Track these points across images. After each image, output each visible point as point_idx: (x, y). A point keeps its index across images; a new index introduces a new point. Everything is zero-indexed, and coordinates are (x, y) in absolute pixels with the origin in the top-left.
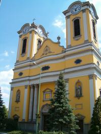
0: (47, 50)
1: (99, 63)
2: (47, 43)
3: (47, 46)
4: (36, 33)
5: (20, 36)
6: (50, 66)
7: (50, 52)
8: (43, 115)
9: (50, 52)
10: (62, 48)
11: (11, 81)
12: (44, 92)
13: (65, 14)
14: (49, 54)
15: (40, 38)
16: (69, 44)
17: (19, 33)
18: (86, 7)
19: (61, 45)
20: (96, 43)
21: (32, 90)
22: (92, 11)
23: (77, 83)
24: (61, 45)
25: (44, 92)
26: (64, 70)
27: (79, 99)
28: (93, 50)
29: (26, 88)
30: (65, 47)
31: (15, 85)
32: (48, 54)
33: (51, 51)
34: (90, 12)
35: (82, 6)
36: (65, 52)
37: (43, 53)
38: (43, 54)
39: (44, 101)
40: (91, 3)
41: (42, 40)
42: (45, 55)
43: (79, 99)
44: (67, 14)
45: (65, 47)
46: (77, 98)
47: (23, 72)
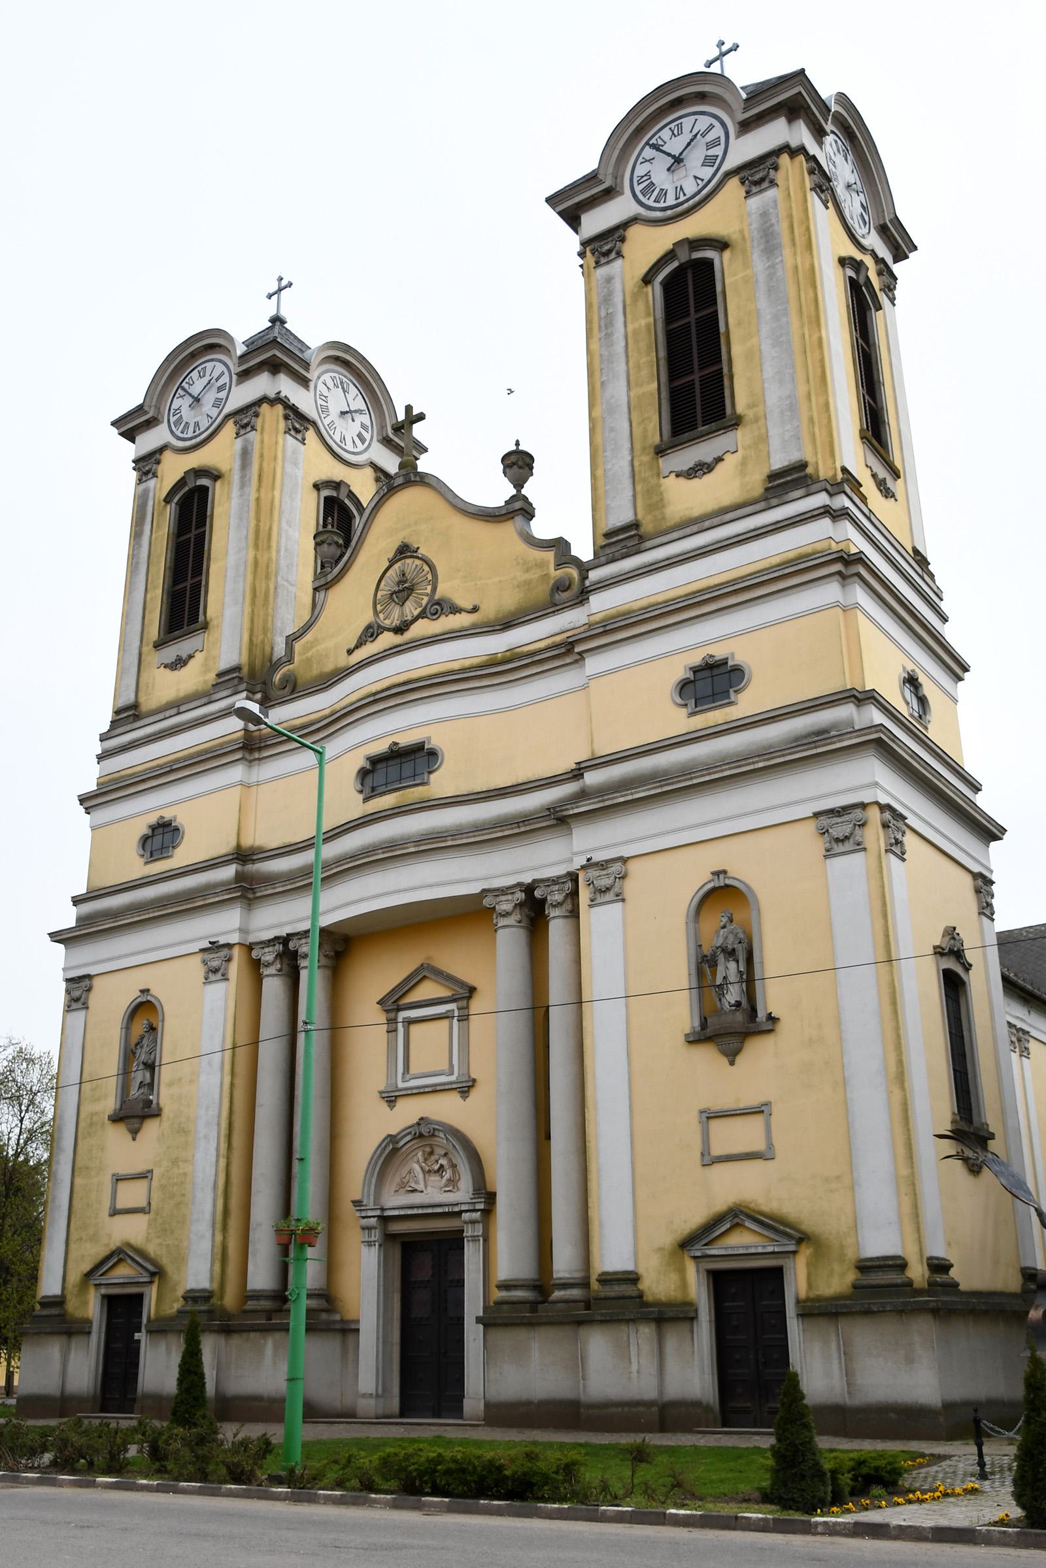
0: (404, 591)
1: (928, 689)
2: (408, 500)
3: (405, 551)
4: (298, 421)
5: (146, 465)
6: (435, 743)
7: (440, 607)
8: (389, 1238)
9: (440, 607)
10: (550, 556)
11: (68, 918)
12: (393, 1003)
13: (572, 218)
14: (422, 628)
15: (338, 472)
16: (621, 515)
17: (130, 436)
18: (775, 133)
19: (541, 528)
20: (888, 493)
21: (274, 987)
22: (843, 171)
23: (893, 493)
24: (541, 528)
25: (393, 1003)
26: (577, 773)
27: (732, 1056)
28: (859, 559)
29: (214, 973)
30: (583, 550)
31: (93, 956)
32: (422, 628)
33: (443, 590)
34: (823, 184)
35: (746, 126)
36: (583, 596)
37: (367, 617)
38: (371, 633)
39: (391, 1098)
40: (898, 281)
41: (364, 487)
42: (387, 640)
43: (732, 1056)
44: (597, 221)
45: (583, 550)
46: (707, 1055)
47: (182, 816)
